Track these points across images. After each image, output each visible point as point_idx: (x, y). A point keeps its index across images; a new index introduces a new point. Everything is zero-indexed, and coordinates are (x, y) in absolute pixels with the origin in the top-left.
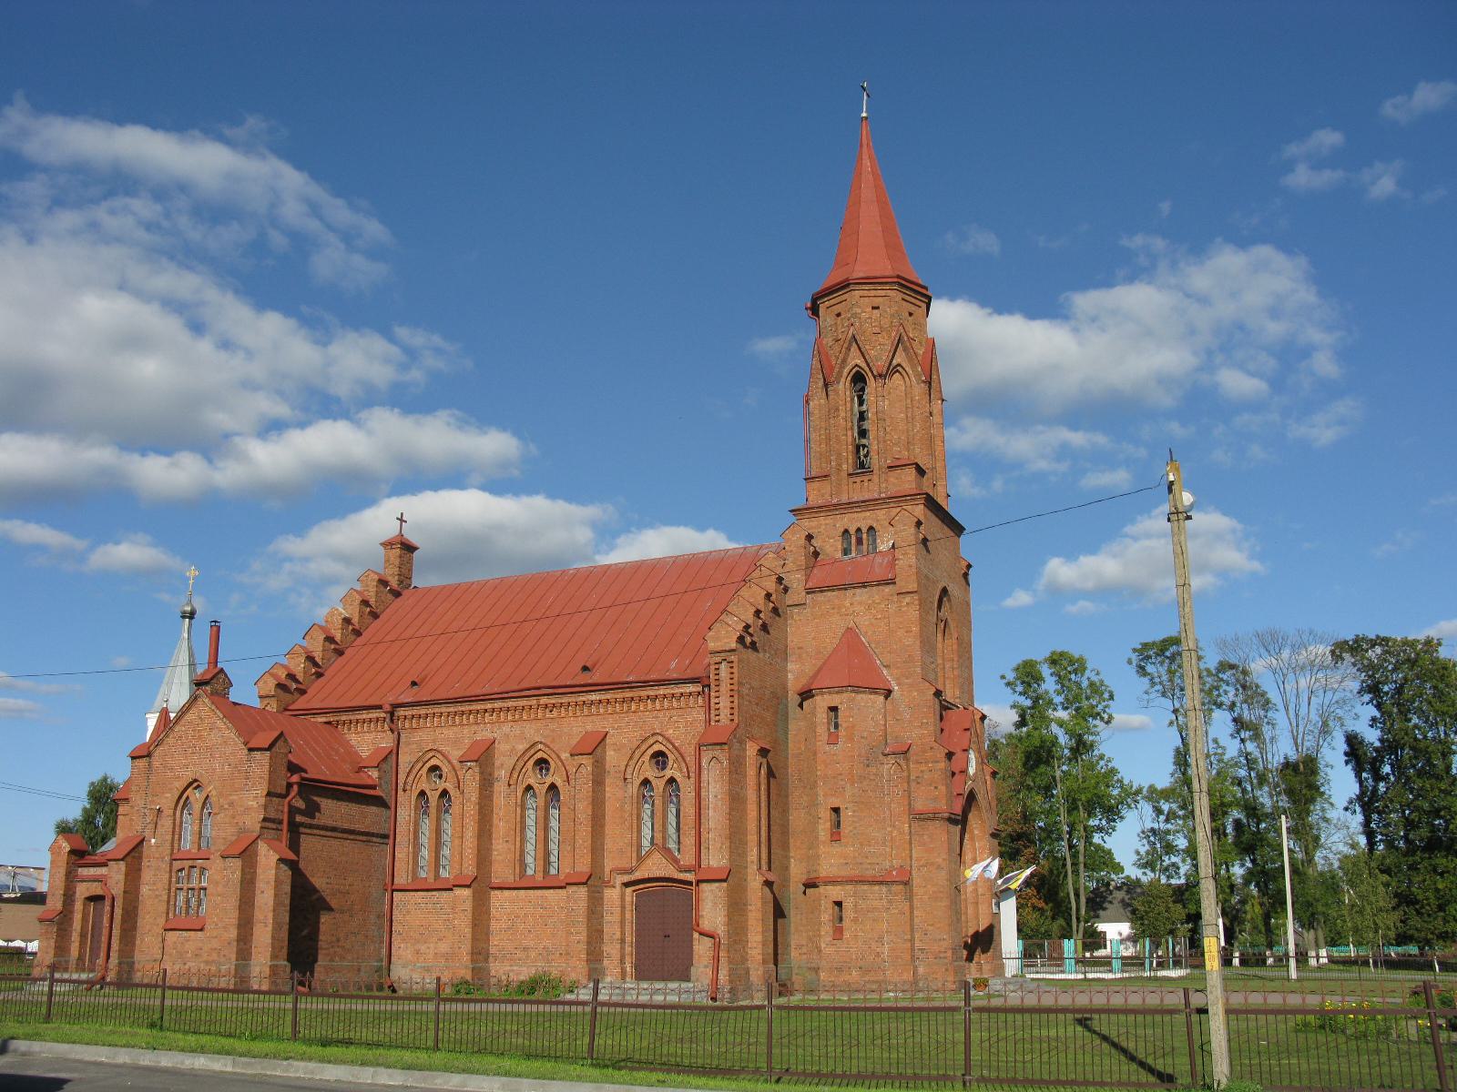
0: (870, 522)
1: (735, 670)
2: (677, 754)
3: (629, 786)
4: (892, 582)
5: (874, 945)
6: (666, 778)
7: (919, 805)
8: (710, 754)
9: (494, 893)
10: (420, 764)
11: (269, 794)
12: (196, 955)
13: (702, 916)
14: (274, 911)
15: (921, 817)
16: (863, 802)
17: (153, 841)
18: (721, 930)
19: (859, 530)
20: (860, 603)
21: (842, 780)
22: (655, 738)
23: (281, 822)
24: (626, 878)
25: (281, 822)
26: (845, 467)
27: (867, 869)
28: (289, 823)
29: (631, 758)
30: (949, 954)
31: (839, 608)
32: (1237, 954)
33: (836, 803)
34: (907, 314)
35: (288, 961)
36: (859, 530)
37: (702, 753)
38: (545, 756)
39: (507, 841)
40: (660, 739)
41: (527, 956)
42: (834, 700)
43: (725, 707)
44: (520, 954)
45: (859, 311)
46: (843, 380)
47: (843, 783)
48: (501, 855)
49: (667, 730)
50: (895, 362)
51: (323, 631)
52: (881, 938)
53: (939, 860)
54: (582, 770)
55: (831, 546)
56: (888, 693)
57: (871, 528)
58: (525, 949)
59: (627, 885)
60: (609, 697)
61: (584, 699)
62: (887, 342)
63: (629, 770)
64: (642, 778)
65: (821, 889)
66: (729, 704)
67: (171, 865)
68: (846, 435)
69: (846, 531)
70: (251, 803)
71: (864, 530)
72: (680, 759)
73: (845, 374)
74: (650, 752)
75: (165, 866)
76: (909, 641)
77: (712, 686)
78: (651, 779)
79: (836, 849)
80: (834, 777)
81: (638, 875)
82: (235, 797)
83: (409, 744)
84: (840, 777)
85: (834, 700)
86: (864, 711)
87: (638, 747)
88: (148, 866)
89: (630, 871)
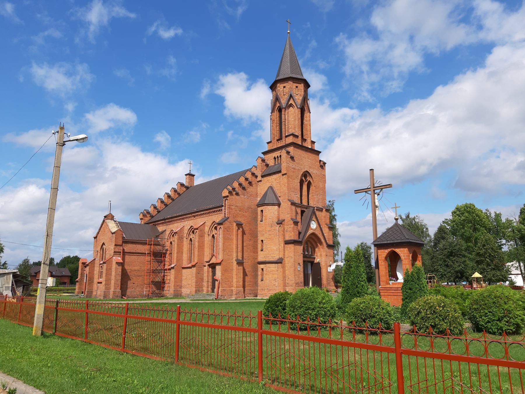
1: (224, 202)
4: (280, 172)
5: (273, 282)
7: (287, 238)
9: (184, 271)
11: (115, 245)
14: (115, 276)
15: (287, 243)
16: (269, 238)
19: (278, 156)
23: (120, 252)
25: (121, 253)
26: (276, 138)
27: (270, 258)
28: (123, 252)
30: (294, 285)
32: (443, 284)
34: (295, 87)
35: (120, 290)
36: (278, 156)
44: (188, 286)
46: (276, 111)
50: (290, 103)
51: (290, 201)
52: (275, 279)
53: (292, 255)
55: (271, 163)
56: (279, 205)
58: (189, 284)
62: (287, 97)
63: (210, 232)
67: (99, 266)
68: (277, 128)
73: (276, 109)
75: (98, 266)
76: (285, 189)
79: (262, 252)
86: (271, 212)
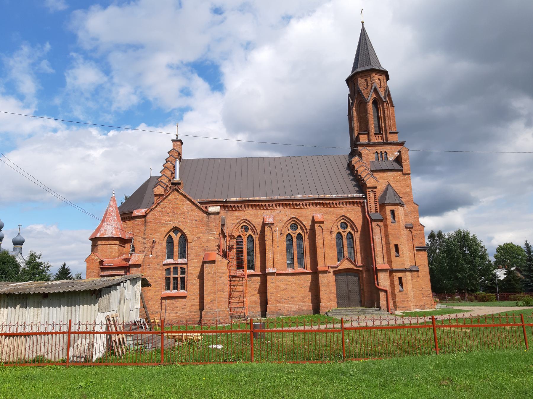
0: (385, 150)
6: (347, 232)
10: (239, 224)
12: (183, 308)
13: (380, 283)
17: (151, 256)
18: (388, 288)
19: (381, 152)
21: (398, 235)
36: (381, 152)
39: (281, 255)
41: (294, 300)
43: (373, 207)
45: (375, 79)
48: (279, 260)
49: (347, 215)
57: (385, 152)
58: (292, 297)
69: (377, 152)
70: (211, 237)
71: (383, 152)
74: (340, 222)
78: (341, 232)
80: (395, 234)
82: (201, 235)
83: (232, 216)
84: (397, 234)
85: (393, 208)
88: (149, 268)
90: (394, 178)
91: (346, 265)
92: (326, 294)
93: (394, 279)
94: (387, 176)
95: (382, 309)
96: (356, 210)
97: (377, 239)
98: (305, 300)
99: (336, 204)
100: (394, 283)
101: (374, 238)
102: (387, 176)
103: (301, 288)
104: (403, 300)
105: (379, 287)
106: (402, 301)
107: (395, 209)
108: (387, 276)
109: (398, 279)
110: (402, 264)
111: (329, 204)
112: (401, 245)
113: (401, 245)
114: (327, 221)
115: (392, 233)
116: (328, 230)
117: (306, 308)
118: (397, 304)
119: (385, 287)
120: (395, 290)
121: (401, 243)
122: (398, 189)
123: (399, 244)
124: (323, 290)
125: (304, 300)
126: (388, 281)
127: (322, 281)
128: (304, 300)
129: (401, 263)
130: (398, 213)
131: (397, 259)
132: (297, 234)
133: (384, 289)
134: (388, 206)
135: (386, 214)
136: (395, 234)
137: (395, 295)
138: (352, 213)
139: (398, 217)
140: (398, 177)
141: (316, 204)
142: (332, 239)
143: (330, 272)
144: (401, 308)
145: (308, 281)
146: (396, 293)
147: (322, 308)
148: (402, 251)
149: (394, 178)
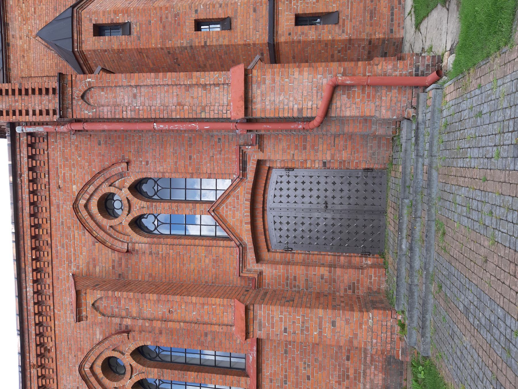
2: (97, 182)
3: (137, 246)
8: (78, 103)
13: (300, 110)
20: (21, 29)
21: (167, 18)
22: (81, 208)
24: (251, 255)
29: (103, 243)
31: (24, 51)
33: (190, 25)
37: (77, 116)
38: (99, 363)
40: (83, 202)
42: (87, 28)
47: (169, 15)
49: (73, 193)
54: (102, 305)
59: (258, 259)
60: (30, 269)
61: (31, 304)
63: (118, 245)
64: (129, 230)
65: (282, 39)
66: (37, 97)
72: (107, 175)
74: (99, 217)
77: (13, 119)
78: (130, 218)
80: (164, 27)
81: (247, 238)
85: (87, 28)
87: (90, 232)
89: (242, 247)
90: (26, 20)
91: (238, 214)
92: (334, 324)
93: (299, 42)
94: (21, 38)
95: (412, 112)
96: (60, 161)
97: (137, 103)
98: (351, 372)
99: (37, 226)
100: (313, 41)
101: (129, 115)
102: (21, 38)
103: (308, 378)
104: (368, 15)
105: (318, 114)
106: (371, 18)
107: (91, 20)
108: (277, 79)
109: (299, 27)
110: (255, 10)
111: (36, 248)
112: (196, 11)
113: (196, 11)
114: (94, 260)
115: (161, 37)
116: (123, 261)
117: (381, 376)
118: (381, 36)
119: (319, 88)
120: (333, 41)
121: (190, 8)
122: (55, 9)
123: (194, 17)
124: (320, 333)
125: (352, 376)
126: (296, 74)
127: (285, 330)
128: (352, 376)
129: (252, 16)
130: (104, 12)
131: (237, 24)
132: (134, 363)
133: (325, 94)
134: (80, 42)
135: (106, 51)
136: (164, 27)
137: (350, 40)
138: (67, 175)
139: (116, 12)
140: (22, 8)
141: (37, 293)
142: (151, 253)
143: (261, 273)
144: (396, 22)
145: (286, 352)
146: (345, 37)
147: (389, 347)
148: (214, 6)
149: (26, 20)
